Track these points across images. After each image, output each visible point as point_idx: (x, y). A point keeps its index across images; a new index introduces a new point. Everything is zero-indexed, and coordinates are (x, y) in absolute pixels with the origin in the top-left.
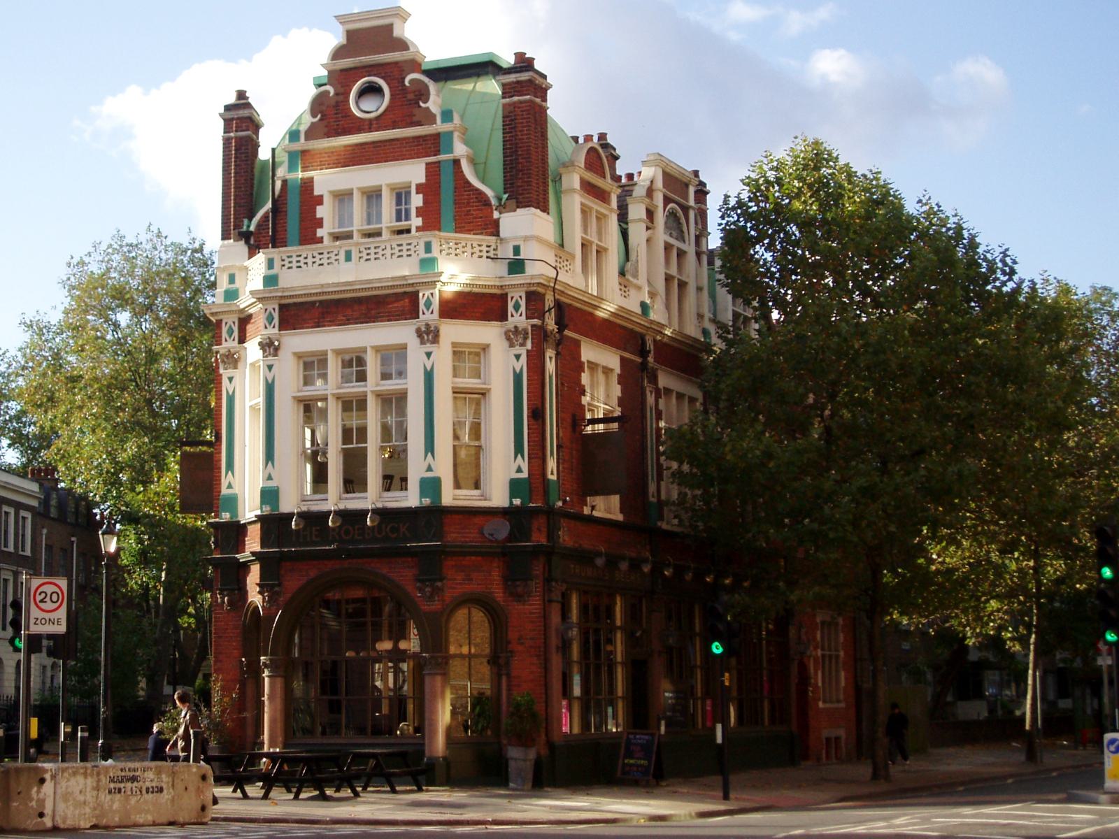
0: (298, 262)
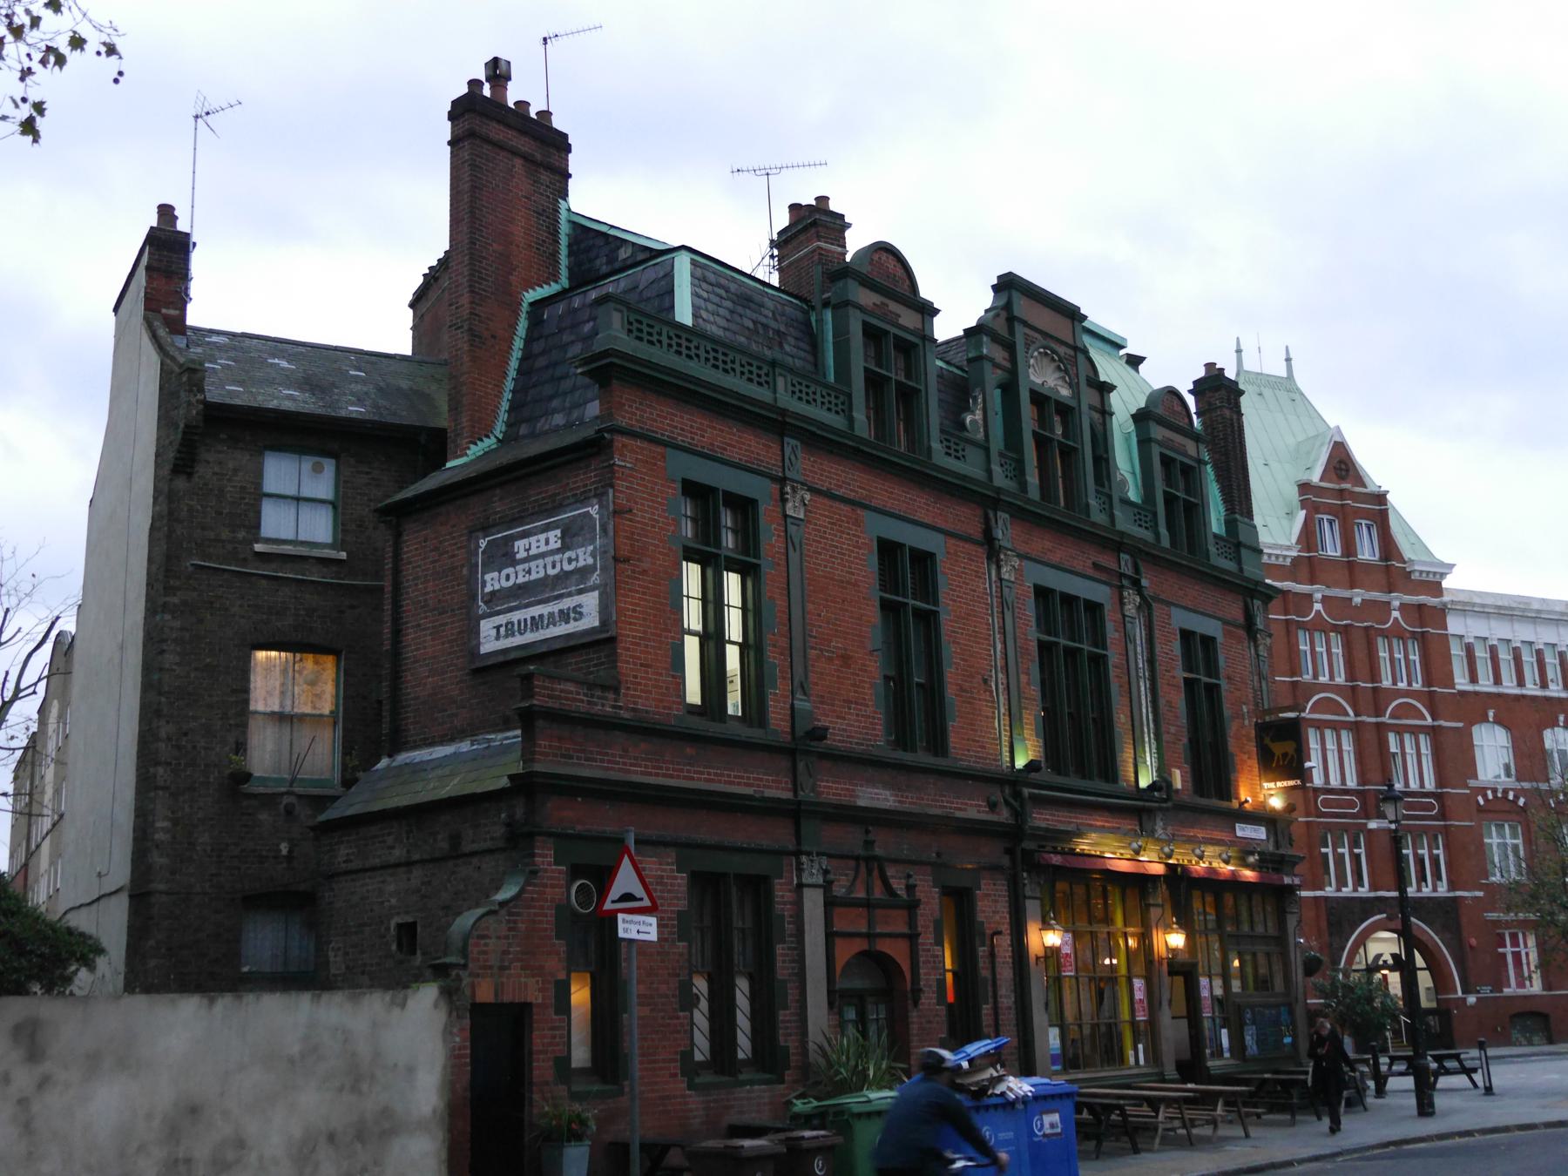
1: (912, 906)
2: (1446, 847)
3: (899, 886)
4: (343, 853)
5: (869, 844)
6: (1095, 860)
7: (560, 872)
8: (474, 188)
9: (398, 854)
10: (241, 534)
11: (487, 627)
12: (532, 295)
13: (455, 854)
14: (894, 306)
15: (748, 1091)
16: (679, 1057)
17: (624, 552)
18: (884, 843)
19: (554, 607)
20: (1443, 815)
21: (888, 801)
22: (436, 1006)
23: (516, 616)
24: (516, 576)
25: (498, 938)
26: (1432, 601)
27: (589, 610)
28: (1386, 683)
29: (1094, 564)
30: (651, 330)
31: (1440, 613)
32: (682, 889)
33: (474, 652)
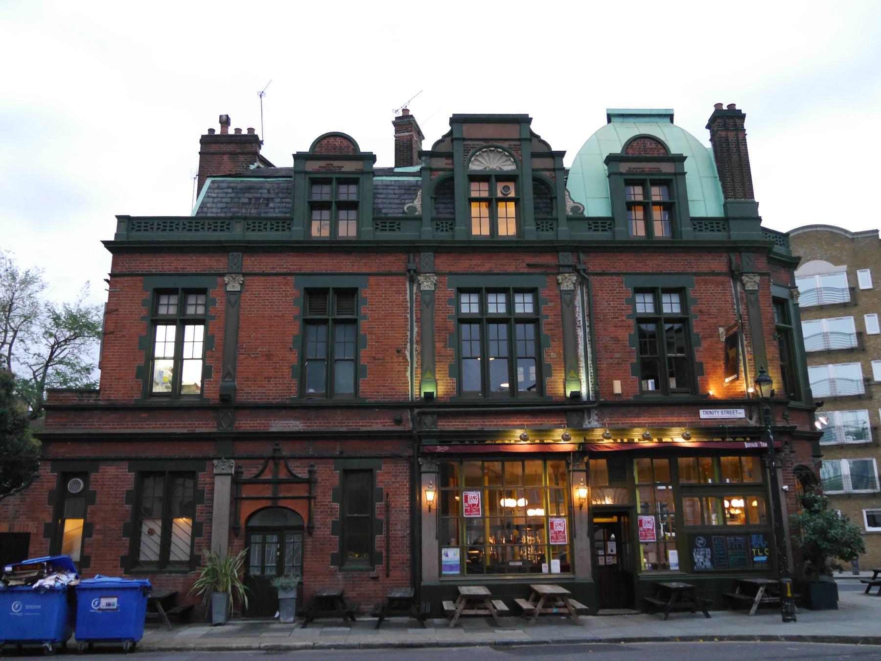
0: (283, 226)
6: (501, 446)
7: (54, 476)
14: (336, 163)
15: (167, 576)
16: (120, 558)
21: (297, 426)
25: (15, 505)
29: (527, 265)
30: (718, 225)
32: (132, 480)
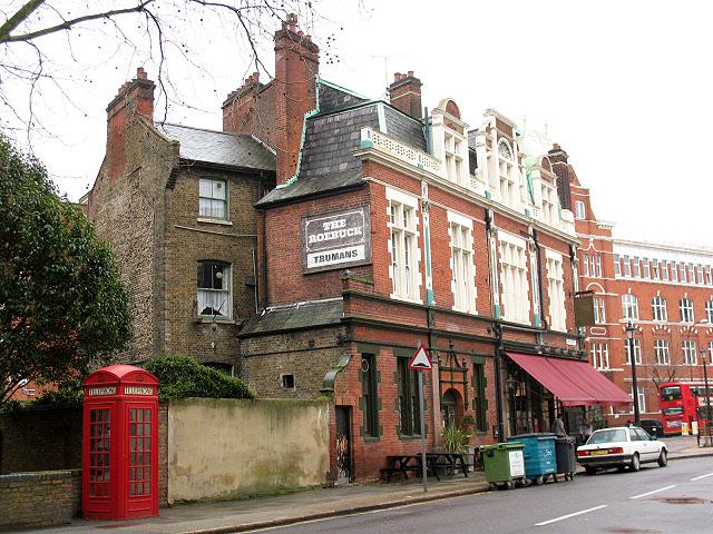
1: (465, 371)
2: (609, 349)
3: (460, 363)
4: (252, 346)
5: (451, 346)
8: (287, 70)
9: (283, 348)
10: (192, 214)
11: (311, 258)
12: (307, 115)
13: (311, 347)
17: (374, 230)
18: (458, 346)
19: (344, 251)
20: (608, 335)
22: (231, 414)
23: (324, 253)
24: (326, 237)
26: (607, 238)
27: (360, 254)
28: (587, 276)
31: (611, 243)
33: (304, 267)
